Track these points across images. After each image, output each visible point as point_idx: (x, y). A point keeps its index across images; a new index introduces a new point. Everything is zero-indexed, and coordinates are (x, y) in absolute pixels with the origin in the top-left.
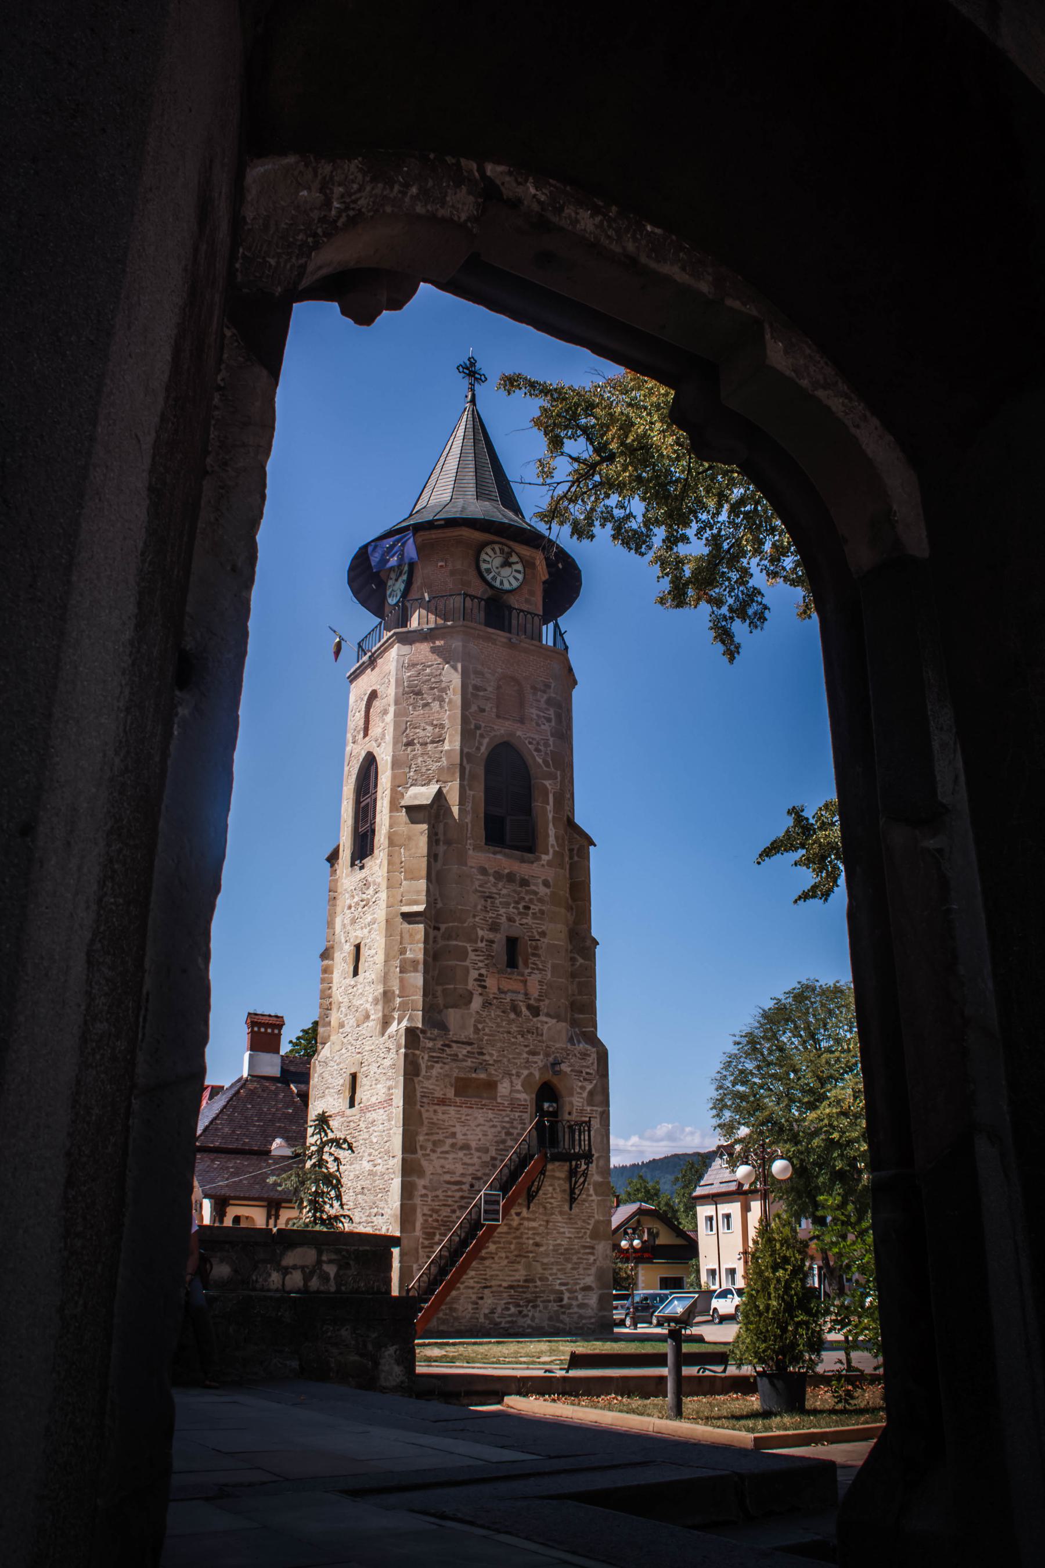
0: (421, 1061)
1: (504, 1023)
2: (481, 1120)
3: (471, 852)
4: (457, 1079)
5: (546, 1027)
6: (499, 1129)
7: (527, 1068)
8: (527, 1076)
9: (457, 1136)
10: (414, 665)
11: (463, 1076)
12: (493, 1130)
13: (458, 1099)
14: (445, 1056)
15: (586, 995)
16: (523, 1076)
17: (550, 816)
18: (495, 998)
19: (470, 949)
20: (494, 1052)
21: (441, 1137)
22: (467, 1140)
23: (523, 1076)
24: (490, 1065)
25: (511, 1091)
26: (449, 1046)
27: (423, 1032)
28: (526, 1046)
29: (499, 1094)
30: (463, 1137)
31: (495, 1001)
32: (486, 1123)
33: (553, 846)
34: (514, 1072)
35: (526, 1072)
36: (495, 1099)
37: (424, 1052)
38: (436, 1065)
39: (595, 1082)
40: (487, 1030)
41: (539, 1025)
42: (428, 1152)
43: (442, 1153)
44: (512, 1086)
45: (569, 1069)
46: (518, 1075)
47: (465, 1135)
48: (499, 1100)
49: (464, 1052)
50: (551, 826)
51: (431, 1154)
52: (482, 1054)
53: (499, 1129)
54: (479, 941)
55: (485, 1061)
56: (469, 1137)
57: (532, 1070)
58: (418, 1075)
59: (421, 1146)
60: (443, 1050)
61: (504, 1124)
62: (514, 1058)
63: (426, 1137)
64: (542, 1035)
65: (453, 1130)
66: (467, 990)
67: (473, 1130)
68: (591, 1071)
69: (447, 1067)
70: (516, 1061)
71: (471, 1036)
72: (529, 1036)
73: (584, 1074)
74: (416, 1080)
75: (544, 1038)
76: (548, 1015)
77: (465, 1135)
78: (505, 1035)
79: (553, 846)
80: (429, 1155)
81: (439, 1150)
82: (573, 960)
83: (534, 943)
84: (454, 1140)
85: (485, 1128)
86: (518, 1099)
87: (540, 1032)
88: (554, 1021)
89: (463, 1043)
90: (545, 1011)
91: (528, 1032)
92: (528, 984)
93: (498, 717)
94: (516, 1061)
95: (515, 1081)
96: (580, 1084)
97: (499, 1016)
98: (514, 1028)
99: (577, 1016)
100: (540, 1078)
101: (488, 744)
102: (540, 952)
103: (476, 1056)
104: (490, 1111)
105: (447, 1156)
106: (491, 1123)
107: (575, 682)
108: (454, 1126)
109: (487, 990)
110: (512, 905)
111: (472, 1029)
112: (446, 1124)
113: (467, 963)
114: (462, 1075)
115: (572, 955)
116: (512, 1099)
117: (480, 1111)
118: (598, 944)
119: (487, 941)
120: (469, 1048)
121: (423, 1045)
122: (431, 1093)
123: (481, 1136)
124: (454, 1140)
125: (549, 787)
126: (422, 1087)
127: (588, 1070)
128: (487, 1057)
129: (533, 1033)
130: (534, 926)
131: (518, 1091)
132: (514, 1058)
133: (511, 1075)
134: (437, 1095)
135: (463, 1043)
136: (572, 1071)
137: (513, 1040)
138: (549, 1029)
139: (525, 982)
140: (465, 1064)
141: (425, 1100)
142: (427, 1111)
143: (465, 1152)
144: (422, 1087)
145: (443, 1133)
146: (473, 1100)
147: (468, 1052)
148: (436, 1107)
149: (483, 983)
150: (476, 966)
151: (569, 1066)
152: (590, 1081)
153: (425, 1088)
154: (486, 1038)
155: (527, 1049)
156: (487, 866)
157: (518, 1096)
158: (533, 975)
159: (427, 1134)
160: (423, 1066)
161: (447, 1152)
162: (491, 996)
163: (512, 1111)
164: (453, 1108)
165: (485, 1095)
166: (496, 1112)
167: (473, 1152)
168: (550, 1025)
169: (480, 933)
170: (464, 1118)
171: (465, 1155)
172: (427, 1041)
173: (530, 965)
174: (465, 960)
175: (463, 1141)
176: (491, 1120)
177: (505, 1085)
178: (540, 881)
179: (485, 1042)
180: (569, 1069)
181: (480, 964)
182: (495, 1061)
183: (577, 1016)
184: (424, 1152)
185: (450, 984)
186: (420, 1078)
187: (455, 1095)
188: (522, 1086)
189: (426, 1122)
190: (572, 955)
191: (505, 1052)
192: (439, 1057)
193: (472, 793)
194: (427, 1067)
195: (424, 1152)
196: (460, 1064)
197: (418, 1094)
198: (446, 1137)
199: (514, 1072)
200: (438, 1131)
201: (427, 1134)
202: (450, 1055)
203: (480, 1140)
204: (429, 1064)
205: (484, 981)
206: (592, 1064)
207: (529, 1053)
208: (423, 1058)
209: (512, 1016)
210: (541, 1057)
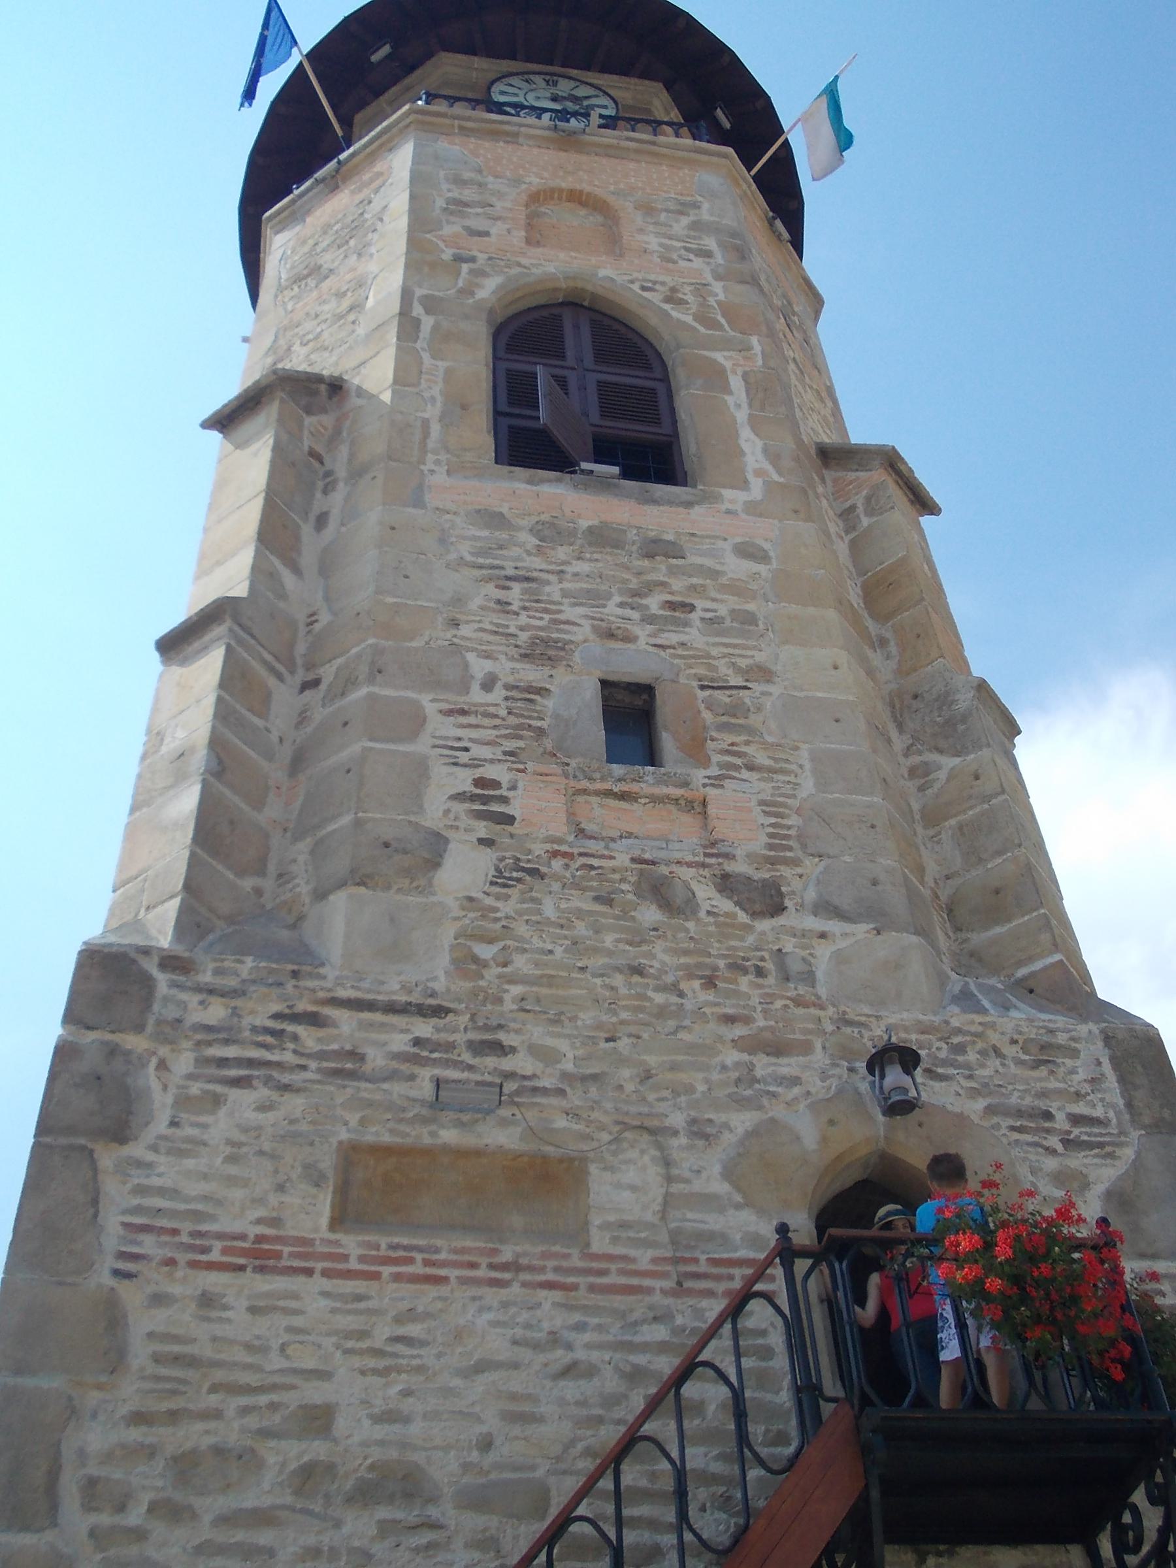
0: (151, 1077)
1: (609, 940)
2: (497, 1345)
3: (440, 478)
4: (351, 1154)
5: (823, 953)
6: (611, 1383)
7: (742, 1103)
8: (753, 1133)
9: (341, 1424)
10: (304, 242)
11: (386, 1138)
12: (571, 1389)
13: (352, 1244)
14: (288, 1057)
15: (999, 853)
16: (728, 1138)
17: (742, 416)
18: (555, 854)
19: (430, 708)
20: (563, 1045)
21: (232, 1433)
22: (404, 1445)
23: (728, 1138)
24: (545, 1091)
25: (668, 1201)
26: (313, 1020)
27: (170, 962)
28: (730, 1020)
29: (596, 1220)
30: (380, 1432)
31: (557, 864)
32: (525, 1354)
33: (759, 473)
34: (677, 1119)
35: (742, 1121)
36: (579, 1234)
37: (170, 1041)
38: (234, 1094)
39: (1128, 1153)
40: (521, 963)
41: (789, 945)
42: (135, 1517)
43: (226, 1520)
44: (669, 1179)
45: (980, 1104)
46: (701, 1132)
47: (388, 1417)
48: (600, 1243)
49: (399, 1042)
50: (746, 435)
51: (158, 1529)
52: (499, 1049)
53: (611, 1383)
54: (475, 687)
55: (511, 1075)
56: (415, 1429)
57: (778, 1111)
58: (120, 1134)
59: (91, 1487)
60: (278, 1034)
61: (640, 1359)
62: (674, 1067)
63: (135, 1434)
64: (809, 977)
65: (315, 1393)
66: (416, 826)
67: (448, 1392)
68: (1098, 1112)
69: (296, 1104)
70: (683, 1077)
71: (439, 985)
72: (744, 983)
73: (1061, 1122)
74: (107, 1157)
75: (822, 991)
76: (826, 908)
77: (388, 1417)
78: (618, 980)
79: (738, 406)
80: (139, 1535)
81: (212, 1505)
82: (921, 772)
83: (722, 696)
84: (318, 1449)
85: (517, 1383)
86: (709, 1237)
87: (795, 966)
88: (862, 929)
89: (392, 1008)
90: (811, 895)
91: (738, 968)
92: (712, 810)
93: (528, 242)
94: (683, 1077)
95: (686, 1162)
96: (1051, 1164)
97: (580, 914)
98: (660, 956)
99: (978, 938)
100: (824, 1140)
101: (501, 287)
102: (754, 720)
103: (467, 1057)
104: (549, 1298)
105: (264, 1537)
106: (560, 1357)
107: (816, 301)
108: (323, 1375)
109: (516, 828)
110: (617, 599)
111: (444, 960)
112: (276, 1362)
113: (422, 746)
114: (379, 1134)
115: (915, 760)
116: (675, 1237)
117: (492, 1296)
118: (1019, 732)
119: (508, 687)
120: (424, 1028)
121: (171, 1013)
122: (197, 1216)
123: (492, 1423)
124: (318, 1449)
125: (728, 365)
126: (141, 1190)
127: (1080, 1109)
128: (521, 1063)
129: (760, 972)
130: (715, 652)
131: (708, 1201)
132: (674, 1067)
133: (657, 1133)
134: (226, 1224)
135: (392, 1008)
136: (990, 1110)
137: (659, 998)
138: (840, 958)
139: (699, 808)
140: (398, 1089)
141: (148, 1245)
142: (159, 1300)
143: (384, 1512)
144: (141, 1190)
145: (245, 1411)
146: (446, 1245)
147: (417, 1042)
148: (214, 1280)
149: (495, 807)
150: (464, 757)
151: (974, 1093)
152: (1105, 1150)
153: (161, 1192)
154: (516, 990)
155: (739, 1031)
156: (505, 510)
157: (713, 1222)
158: (727, 783)
159: (139, 1418)
160: (162, 1103)
161: (262, 1518)
162: (539, 849)
163: (679, 1290)
164: (320, 1283)
165: (517, 1221)
166: (582, 1296)
167: (446, 1512)
168: (842, 944)
169: (479, 667)
170: (383, 1332)
171: (385, 1529)
172: (193, 999)
173: (716, 758)
174: (413, 735)
175: (376, 1454)
176: (554, 1340)
177: (630, 1175)
178: (727, 546)
179: (509, 1005)
180: (980, 1104)
181: (485, 752)
182: (565, 1076)
183: (978, 938)
184: (104, 1519)
185: (334, 818)
186: (136, 1150)
187: (336, 1223)
188: (728, 1174)
189: (140, 1353)
190: (915, 760)
191: (624, 1044)
192: (251, 1063)
193: (442, 365)
194: (183, 1102)
195: (104, 1519)
196: (366, 1090)
197: (112, 1222)
198: (265, 1433)
199: (677, 1119)
200: (213, 1400)
201: (139, 1418)
202: (322, 1056)
203: (486, 1444)
204: (195, 1089)
205: (504, 800)
206: (1095, 1081)
207: (753, 1045)
208: (162, 1065)
209: (650, 914)
210: (819, 1058)
